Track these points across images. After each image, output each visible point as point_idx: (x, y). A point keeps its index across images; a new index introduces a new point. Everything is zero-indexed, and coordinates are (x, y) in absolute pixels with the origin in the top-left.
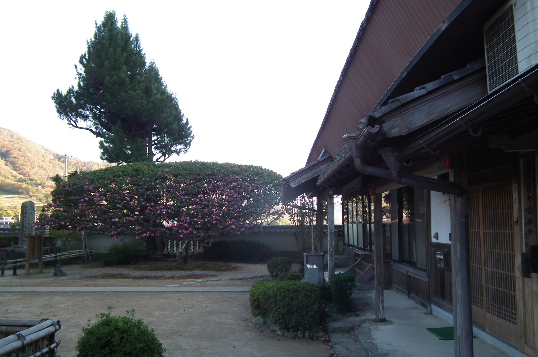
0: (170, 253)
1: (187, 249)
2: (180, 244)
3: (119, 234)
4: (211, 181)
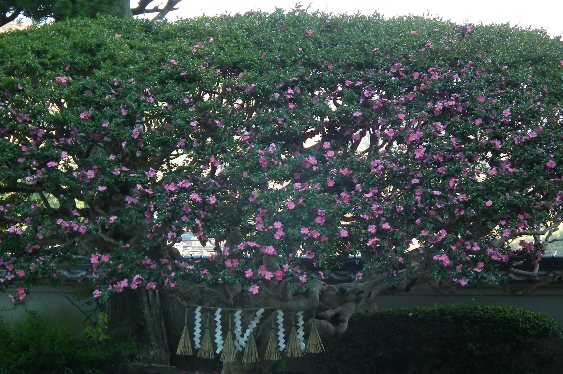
0: (201, 355)
1: (260, 339)
2: (238, 323)
3: (33, 280)
4: (358, 90)
